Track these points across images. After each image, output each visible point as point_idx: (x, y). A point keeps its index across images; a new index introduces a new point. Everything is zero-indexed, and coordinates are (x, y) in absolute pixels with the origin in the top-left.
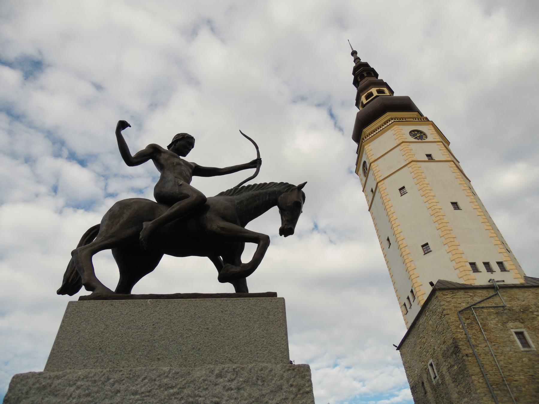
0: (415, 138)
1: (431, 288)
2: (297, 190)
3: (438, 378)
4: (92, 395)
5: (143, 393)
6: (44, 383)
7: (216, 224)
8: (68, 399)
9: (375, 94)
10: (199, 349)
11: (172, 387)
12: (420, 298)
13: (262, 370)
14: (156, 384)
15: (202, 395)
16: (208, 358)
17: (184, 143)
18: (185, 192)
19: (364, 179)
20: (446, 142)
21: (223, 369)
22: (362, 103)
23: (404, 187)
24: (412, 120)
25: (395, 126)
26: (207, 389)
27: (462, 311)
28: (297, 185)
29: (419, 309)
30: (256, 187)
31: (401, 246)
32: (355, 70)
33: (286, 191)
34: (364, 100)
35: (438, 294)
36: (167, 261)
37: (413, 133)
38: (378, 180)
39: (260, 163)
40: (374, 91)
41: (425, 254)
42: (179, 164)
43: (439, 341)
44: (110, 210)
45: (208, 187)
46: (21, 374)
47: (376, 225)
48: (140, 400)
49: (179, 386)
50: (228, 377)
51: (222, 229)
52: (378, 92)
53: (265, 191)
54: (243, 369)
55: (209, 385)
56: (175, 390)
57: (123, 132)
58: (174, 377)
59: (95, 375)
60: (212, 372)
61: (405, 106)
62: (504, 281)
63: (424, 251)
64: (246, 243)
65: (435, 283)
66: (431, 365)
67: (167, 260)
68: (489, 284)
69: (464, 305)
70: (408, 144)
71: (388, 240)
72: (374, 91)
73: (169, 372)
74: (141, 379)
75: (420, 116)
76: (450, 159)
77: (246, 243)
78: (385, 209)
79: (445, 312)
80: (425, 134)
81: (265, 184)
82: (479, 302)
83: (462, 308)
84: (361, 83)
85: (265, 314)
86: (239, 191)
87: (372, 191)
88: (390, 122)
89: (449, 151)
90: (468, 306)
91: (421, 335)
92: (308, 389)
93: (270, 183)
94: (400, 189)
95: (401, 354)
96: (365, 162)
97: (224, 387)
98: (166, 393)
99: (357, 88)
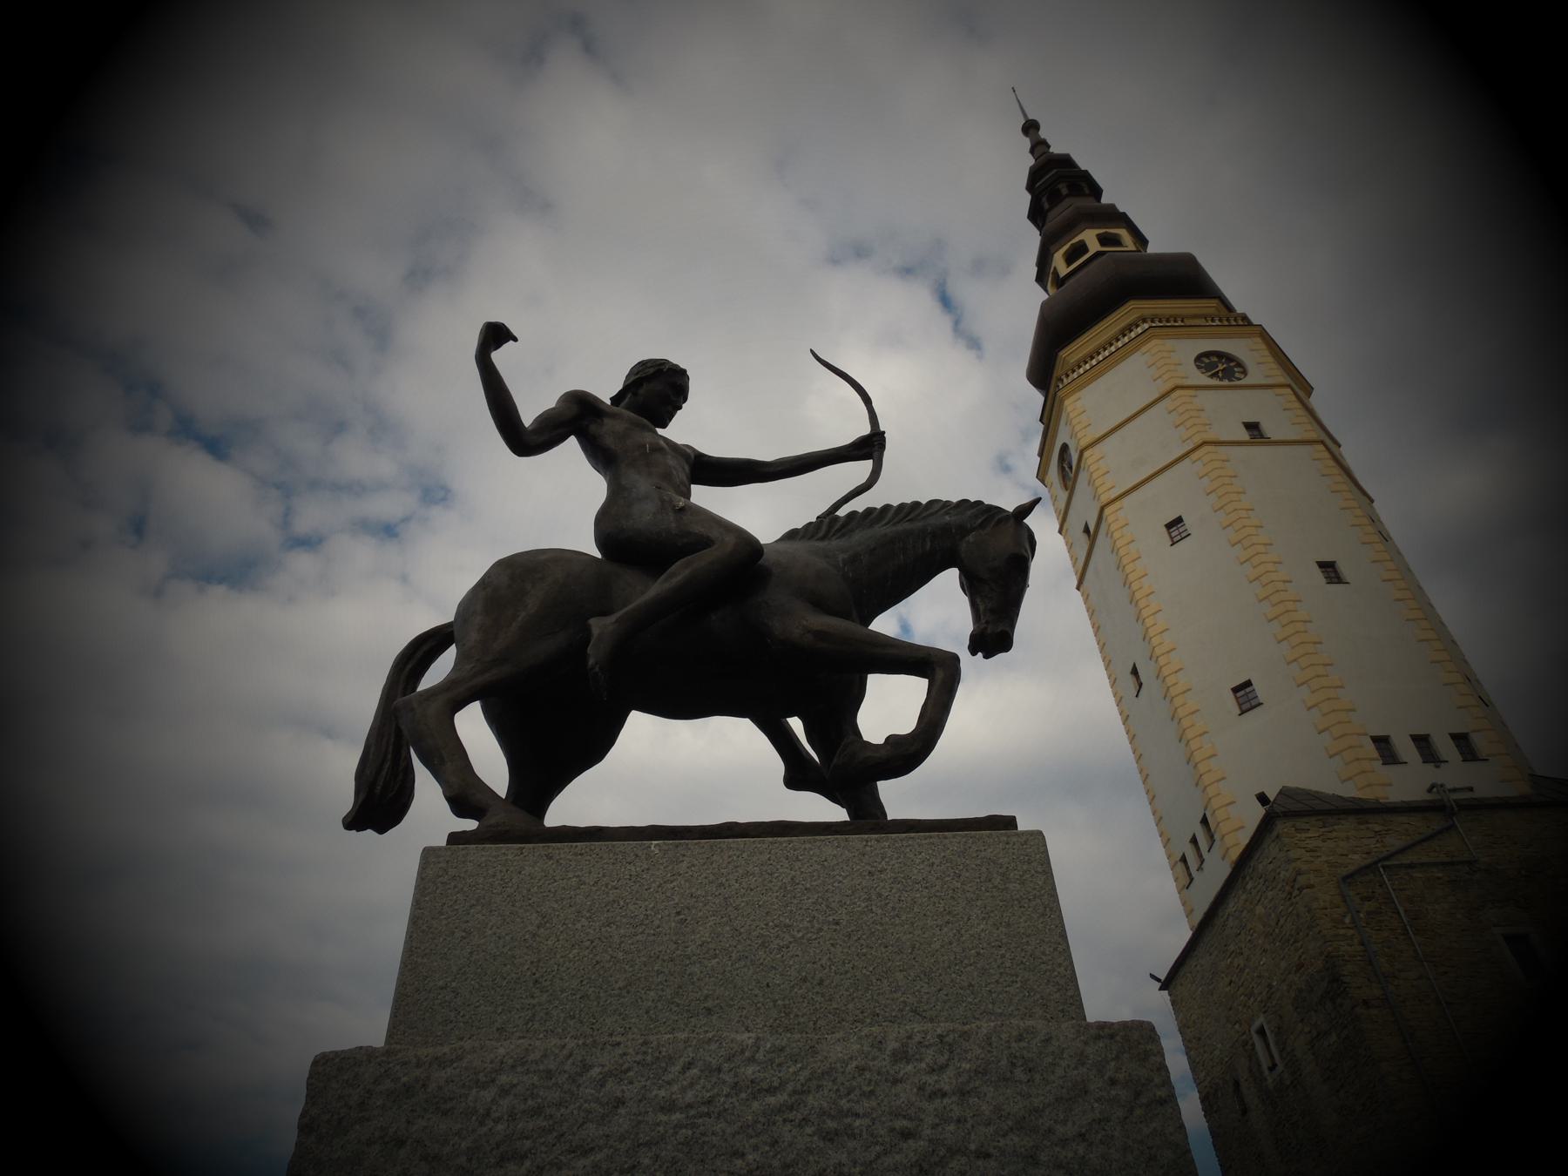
0: (1212, 376)
1: (1259, 811)
2: (1012, 521)
3: (1280, 1067)
4: (548, 1111)
5: (690, 1106)
6: (405, 1079)
7: (805, 623)
8: (482, 1124)
9: (1094, 246)
10: (821, 983)
11: (772, 1091)
12: (1229, 841)
13: (1020, 1039)
14: (724, 1082)
15: (861, 1111)
16: (851, 1006)
17: (659, 388)
18: (698, 529)
19: (1064, 495)
20: (1300, 386)
21: (909, 1037)
22: (1056, 273)
23: (1179, 520)
24: (1202, 322)
25: (1154, 342)
26: (872, 1092)
27: (1350, 876)
28: (1010, 508)
29: (1225, 871)
30: (890, 515)
31: (1173, 692)
32: (1035, 176)
33: (982, 526)
34: (1060, 265)
35: (1281, 827)
36: (642, 732)
37: (1206, 361)
38: (1105, 498)
39: (882, 446)
40: (1090, 238)
41: (1243, 713)
42: (659, 449)
43: (1283, 964)
44: (483, 584)
45: (763, 515)
46: (336, 1053)
47: (1097, 630)
48: (686, 1127)
49: (790, 1087)
50: (928, 1059)
51: (820, 635)
52: (1103, 240)
53: (919, 524)
54: (965, 1035)
55: (877, 1084)
56: (781, 1098)
57: (499, 357)
58: (772, 1061)
59: (545, 1056)
60: (879, 1044)
61: (1182, 281)
62: (1471, 789)
63: (1240, 705)
64: (870, 677)
65: (1271, 796)
66: (1261, 1032)
67: (639, 727)
68: (1428, 797)
69: (1357, 860)
70: (1191, 392)
71: (1135, 672)
72: (1090, 238)
73: (757, 1046)
74: (678, 1068)
75: (1224, 312)
76: (1313, 436)
77: (870, 677)
78: (1126, 583)
79: (1302, 880)
80: (1239, 365)
81: (916, 504)
82: (1403, 851)
83: (1352, 868)
84: (1051, 215)
85: (997, 880)
86: (843, 526)
87: (1087, 530)
88: (1139, 330)
89: (1311, 412)
90: (1369, 861)
91: (1232, 947)
92: (1161, 1093)
93: (932, 503)
94: (1169, 526)
95: (1173, 1002)
96: (1065, 448)
97: (921, 1088)
98: (755, 1105)
99: (1040, 228)
